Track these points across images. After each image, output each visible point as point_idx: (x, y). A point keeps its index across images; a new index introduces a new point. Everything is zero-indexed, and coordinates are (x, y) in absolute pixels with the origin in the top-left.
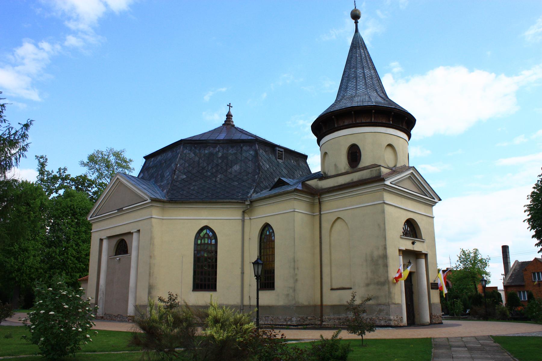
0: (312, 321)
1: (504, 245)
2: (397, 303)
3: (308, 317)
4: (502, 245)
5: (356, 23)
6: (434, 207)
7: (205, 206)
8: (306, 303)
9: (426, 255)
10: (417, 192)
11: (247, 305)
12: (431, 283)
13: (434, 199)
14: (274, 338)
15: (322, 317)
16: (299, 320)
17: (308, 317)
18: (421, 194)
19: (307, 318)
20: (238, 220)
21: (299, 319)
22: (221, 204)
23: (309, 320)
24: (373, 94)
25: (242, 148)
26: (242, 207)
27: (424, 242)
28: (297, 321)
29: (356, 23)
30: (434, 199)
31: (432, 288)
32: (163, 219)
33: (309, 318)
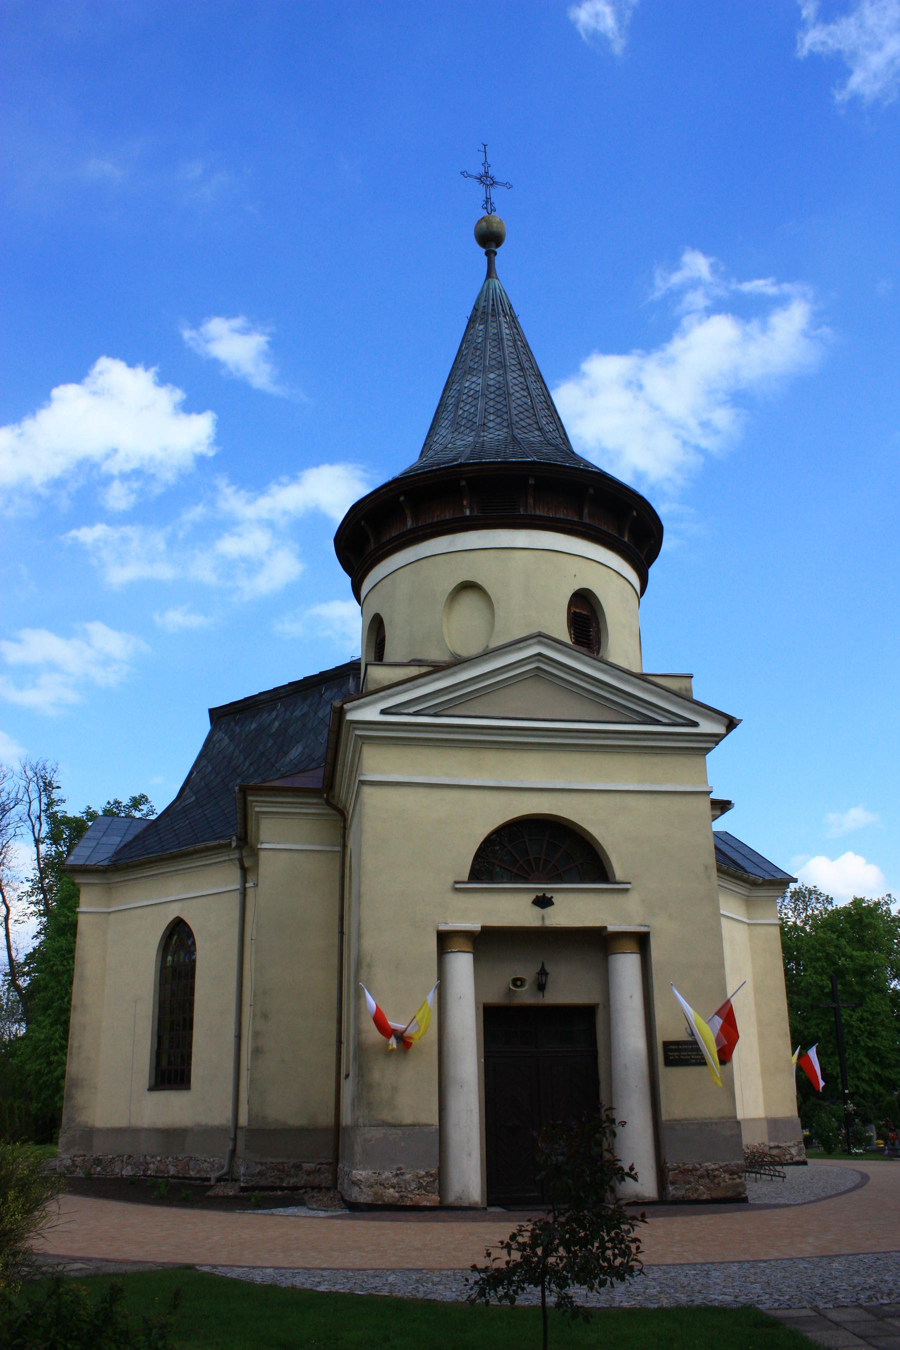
0: (322, 1176)
1: (185, 919)
2: (408, 1120)
3: (304, 1165)
4: (182, 916)
5: (490, 255)
6: (707, 756)
7: (186, 864)
8: (294, 1121)
9: (641, 941)
10: (614, 720)
11: (761, 1119)
12: (666, 1044)
13: (695, 724)
14: (520, 1224)
15: (337, 1163)
16: (260, 1173)
17: (304, 1165)
18: (628, 720)
19: (298, 1167)
20: (210, 898)
21: (259, 1168)
22: (200, 858)
23: (308, 1173)
24: (532, 439)
25: (321, 695)
26: (227, 858)
27: (627, 890)
28: (253, 1176)
29: (490, 255)
30: (695, 724)
31: (669, 1063)
32: (109, 913)
33: (307, 1166)
